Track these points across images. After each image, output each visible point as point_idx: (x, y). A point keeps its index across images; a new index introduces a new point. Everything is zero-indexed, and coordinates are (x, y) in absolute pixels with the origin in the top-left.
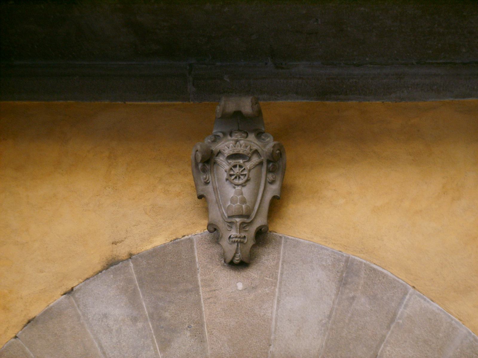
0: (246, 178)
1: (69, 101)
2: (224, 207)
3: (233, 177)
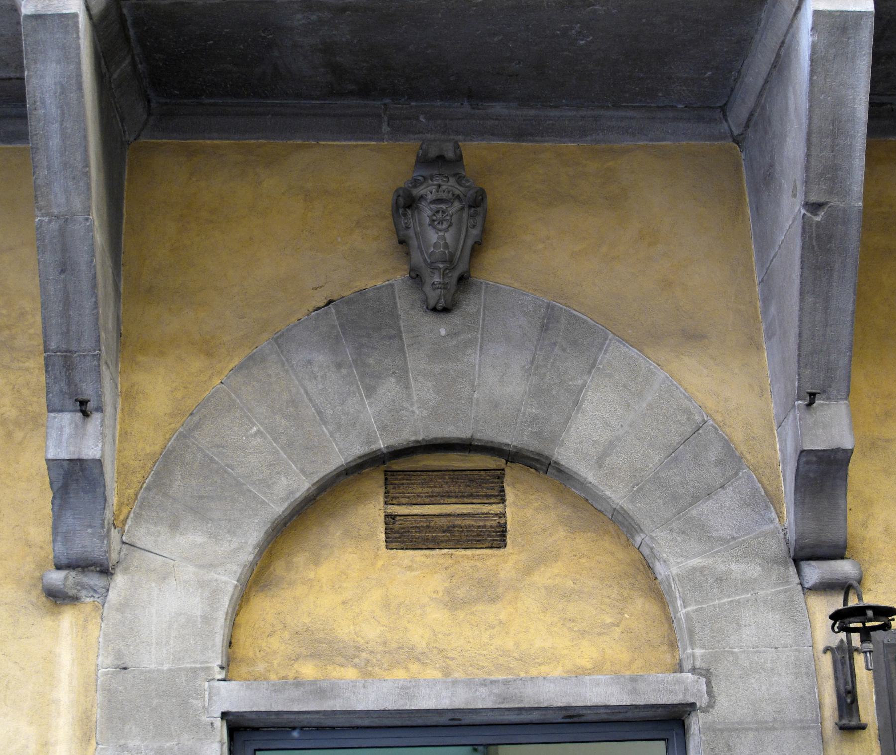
0: (449, 223)
1: (260, 141)
2: (426, 252)
3: (436, 223)
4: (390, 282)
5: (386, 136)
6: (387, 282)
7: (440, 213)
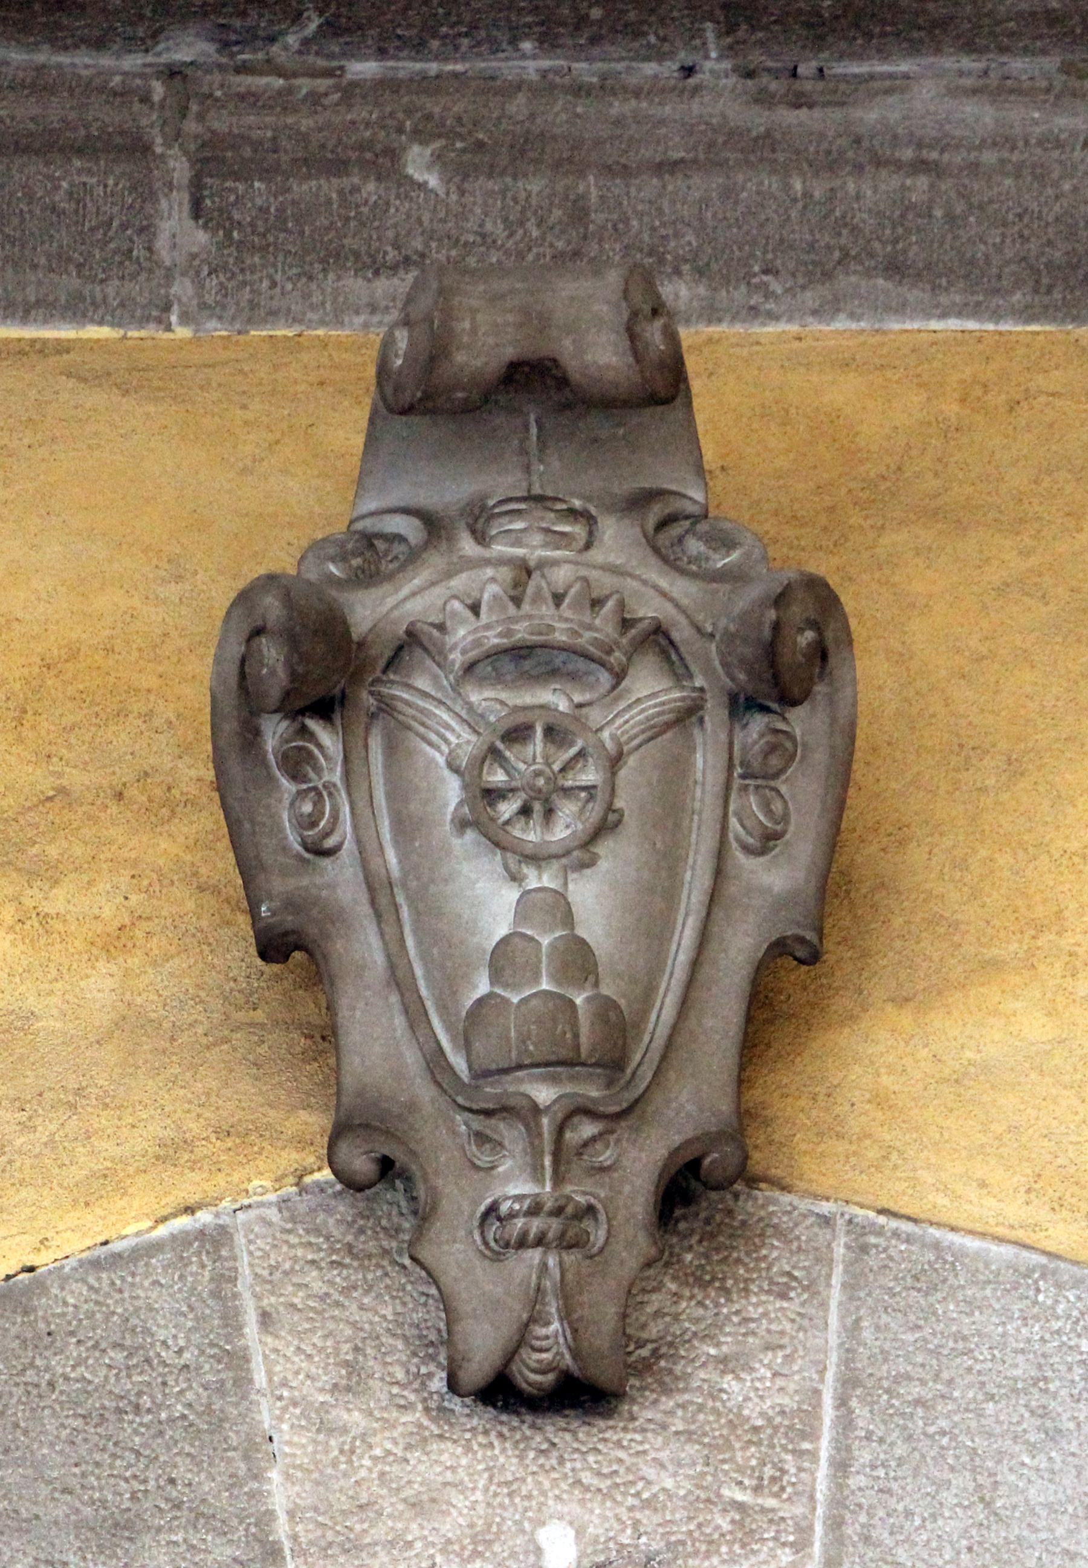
0: (594, 813)
2: (443, 1009)
3: (507, 809)
4: (204, 1217)
5: (182, 288)
6: (183, 1222)
7: (538, 744)
